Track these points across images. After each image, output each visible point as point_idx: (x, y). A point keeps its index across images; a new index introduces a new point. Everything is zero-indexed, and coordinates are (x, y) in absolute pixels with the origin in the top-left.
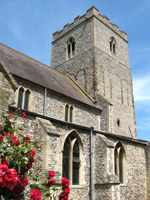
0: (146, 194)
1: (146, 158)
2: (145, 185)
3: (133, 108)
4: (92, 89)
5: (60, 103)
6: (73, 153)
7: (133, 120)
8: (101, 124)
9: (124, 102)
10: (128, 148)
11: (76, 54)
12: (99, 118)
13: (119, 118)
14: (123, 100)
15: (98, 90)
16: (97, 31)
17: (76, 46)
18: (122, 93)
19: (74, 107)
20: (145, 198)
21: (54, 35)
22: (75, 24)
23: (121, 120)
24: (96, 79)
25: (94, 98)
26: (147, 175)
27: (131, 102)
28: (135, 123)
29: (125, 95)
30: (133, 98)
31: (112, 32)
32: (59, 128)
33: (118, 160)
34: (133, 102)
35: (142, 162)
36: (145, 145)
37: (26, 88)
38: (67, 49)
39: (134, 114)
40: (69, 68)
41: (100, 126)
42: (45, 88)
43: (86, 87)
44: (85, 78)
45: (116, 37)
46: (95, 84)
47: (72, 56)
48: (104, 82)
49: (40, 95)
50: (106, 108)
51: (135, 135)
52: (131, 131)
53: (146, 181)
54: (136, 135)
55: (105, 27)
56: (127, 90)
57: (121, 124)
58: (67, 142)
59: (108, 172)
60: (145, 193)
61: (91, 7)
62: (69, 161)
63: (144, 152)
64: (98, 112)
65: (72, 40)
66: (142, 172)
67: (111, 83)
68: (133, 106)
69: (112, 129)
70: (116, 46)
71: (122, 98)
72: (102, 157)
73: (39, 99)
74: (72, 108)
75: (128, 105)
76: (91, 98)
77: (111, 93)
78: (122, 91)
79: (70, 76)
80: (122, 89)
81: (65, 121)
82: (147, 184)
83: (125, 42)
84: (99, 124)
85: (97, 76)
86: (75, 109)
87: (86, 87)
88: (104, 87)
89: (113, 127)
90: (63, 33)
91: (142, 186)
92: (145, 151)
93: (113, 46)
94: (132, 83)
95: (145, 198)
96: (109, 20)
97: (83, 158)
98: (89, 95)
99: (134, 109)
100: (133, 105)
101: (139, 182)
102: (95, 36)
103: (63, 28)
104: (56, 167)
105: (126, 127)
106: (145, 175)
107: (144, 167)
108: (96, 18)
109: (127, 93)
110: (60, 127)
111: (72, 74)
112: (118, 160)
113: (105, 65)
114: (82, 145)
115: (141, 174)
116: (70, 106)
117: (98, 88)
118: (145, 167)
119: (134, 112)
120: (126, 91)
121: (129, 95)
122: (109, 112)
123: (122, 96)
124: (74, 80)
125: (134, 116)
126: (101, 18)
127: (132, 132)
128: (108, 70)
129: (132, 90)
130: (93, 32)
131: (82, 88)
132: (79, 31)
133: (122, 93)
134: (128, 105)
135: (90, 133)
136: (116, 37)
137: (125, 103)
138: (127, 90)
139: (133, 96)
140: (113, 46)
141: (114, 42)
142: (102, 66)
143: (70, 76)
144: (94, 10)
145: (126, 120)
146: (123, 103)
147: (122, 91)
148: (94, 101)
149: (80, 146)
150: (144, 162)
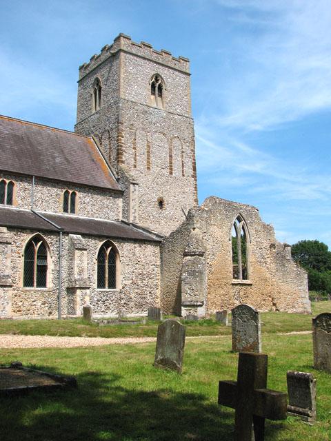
1: (161, 258)
2: (158, 292)
4: (116, 160)
5: (55, 191)
6: (38, 256)
8: (123, 210)
10: (124, 249)
11: (102, 106)
12: (120, 202)
13: (162, 198)
14: (171, 169)
15: (123, 162)
16: (126, 72)
17: (102, 92)
18: (171, 159)
19: (77, 192)
21: (81, 68)
22: (103, 58)
23: (165, 200)
24: (121, 146)
25: (117, 173)
27: (189, 171)
29: (177, 162)
30: (194, 163)
31: (157, 66)
32: (19, 233)
33: (64, 263)
34: (195, 169)
35: (154, 263)
36: (160, 242)
37: (8, 179)
38: (93, 95)
39: (195, 188)
40: (94, 127)
41: (121, 213)
42: (32, 176)
43: (110, 157)
44: (110, 144)
45: (164, 72)
46: (119, 154)
47: (98, 108)
48: (135, 148)
49: (26, 185)
50: (128, 188)
55: (142, 61)
56: (183, 152)
57: (165, 206)
58: (29, 248)
59: (75, 276)
61: (118, 35)
64: (118, 194)
65: (97, 81)
67: (149, 146)
68: (194, 176)
69: (135, 217)
70: (164, 87)
71: (171, 166)
72: (71, 260)
73: (25, 189)
74: (74, 194)
75: (183, 175)
76: (115, 173)
77: (148, 162)
78: (171, 156)
79: (95, 138)
81: (65, 210)
83: (184, 76)
84: (121, 210)
85: (123, 141)
86: (79, 195)
87: (110, 157)
88: (136, 155)
89: (136, 215)
90: (90, 69)
93: (157, 87)
94: (193, 141)
96: (151, 47)
97: (50, 263)
98: (112, 169)
99: (196, 180)
100: (196, 174)
101: (144, 288)
102: (122, 81)
103: (99, 53)
104: (7, 271)
107: (158, 270)
108: (125, 52)
109: (183, 156)
110: (20, 232)
111: (96, 136)
112: (64, 263)
113: (138, 124)
114: (49, 248)
116: (71, 192)
117: (124, 159)
122: (131, 194)
123: (171, 163)
124: (99, 144)
126: (134, 50)
128: (143, 129)
130: (119, 76)
131: (106, 157)
132: (104, 71)
133: (171, 159)
135: (59, 234)
136: (164, 72)
137: (177, 172)
139: (194, 160)
140: (157, 87)
141: (160, 82)
142: (132, 125)
143: (95, 138)
144: (123, 41)
146: (171, 173)
147: (171, 156)
148: (117, 177)
149: (47, 248)
150: (159, 263)
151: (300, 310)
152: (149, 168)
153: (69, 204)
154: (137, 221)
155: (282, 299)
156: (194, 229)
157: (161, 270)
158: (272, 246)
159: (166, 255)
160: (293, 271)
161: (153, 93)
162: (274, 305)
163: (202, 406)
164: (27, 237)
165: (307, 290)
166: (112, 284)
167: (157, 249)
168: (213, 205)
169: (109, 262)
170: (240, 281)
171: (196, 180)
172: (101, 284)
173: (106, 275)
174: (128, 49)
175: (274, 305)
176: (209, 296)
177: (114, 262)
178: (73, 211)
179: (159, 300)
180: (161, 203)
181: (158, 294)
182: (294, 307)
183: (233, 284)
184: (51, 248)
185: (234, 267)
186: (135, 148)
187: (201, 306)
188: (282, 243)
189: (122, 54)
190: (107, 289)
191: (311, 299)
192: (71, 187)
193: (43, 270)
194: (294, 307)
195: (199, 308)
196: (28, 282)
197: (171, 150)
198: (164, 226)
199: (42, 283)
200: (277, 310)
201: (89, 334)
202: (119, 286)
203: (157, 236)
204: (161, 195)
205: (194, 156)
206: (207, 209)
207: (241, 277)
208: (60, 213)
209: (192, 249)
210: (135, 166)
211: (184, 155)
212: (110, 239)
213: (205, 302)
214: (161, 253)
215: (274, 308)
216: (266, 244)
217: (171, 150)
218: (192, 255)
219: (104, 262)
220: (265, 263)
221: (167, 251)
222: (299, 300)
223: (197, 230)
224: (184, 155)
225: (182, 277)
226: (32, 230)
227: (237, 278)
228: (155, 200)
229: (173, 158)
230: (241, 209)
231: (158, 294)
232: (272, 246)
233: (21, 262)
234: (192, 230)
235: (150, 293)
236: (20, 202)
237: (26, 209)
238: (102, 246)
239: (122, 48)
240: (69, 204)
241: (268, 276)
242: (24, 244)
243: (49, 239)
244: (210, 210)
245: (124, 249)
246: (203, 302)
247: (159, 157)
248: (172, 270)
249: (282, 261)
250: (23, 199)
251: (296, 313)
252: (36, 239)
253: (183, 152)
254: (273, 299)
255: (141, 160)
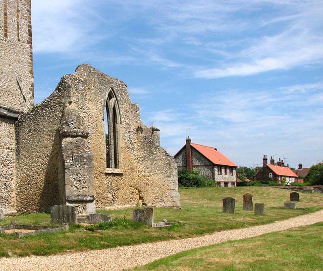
0: (15, 198)
1: (17, 140)
2: (13, 184)
3: (28, 45)
7: (27, 68)
9: (8, 33)
14: (6, 31)
18: (6, 18)
20: (12, 204)
26: (17, 168)
28: (31, 72)
29: (12, 22)
30: (30, 26)
34: (30, 34)
35: (8, 146)
36: (16, 119)
39: (31, 56)
51: (29, 96)
52: (22, 87)
53: (15, 177)
54: (33, 95)
56: (18, 11)
60: (12, 196)
62: (270, 42)
63: (13, 130)
66: (8, 162)
68: (30, 42)
71: (6, 27)
75: (19, 40)
78: (6, 14)
80: (5, 9)
82: (17, 182)
91: (5, 184)
92: (16, 129)
95: (12, 204)
100: (31, 39)
105: (10, 80)
106: (15, 168)
107: (13, 155)
109: (18, 16)
115: (5, 165)
118: (14, 154)
119: (31, 53)
120: (16, 14)
121: (22, 22)
123: (6, 23)
125: (31, 59)
127: (24, 91)
129: (29, 11)
133: (6, 18)
134: (19, 40)
137: (12, 36)
138: (18, 11)
139: (30, 22)
145: (10, 67)
146: (6, 36)
147: (6, 14)
150: (14, 146)
151: (169, 204)
155: (150, 192)
156: (70, 103)
157: (18, 155)
158: (139, 129)
159: (24, 136)
160: (162, 160)
162: (141, 198)
165: (177, 182)
167: (11, 128)
168: (88, 75)
170: (109, 170)
171: (31, 47)
175: (141, 198)
179: (14, 194)
181: (14, 186)
182: (162, 200)
183: (107, 174)
187: (91, 201)
188: (149, 127)
194: (162, 200)
195: (88, 205)
197: (5, 6)
200: (143, 204)
201: (18, 252)
203: (9, 110)
205: (29, 18)
206: (82, 79)
207: (113, 166)
209: (72, 128)
211: (20, 14)
213: (95, 196)
214: (17, 133)
215: (141, 202)
216: (133, 128)
217: (5, 6)
218: (73, 137)
220: (133, 149)
221: (27, 130)
222: (168, 193)
223: (73, 104)
225: (66, 164)
227: (108, 166)
229: (9, 17)
230: (112, 83)
231: (14, 186)
232: (139, 129)
234: (67, 104)
235: (5, 184)
241: (136, 164)
244: (86, 81)
246: (93, 197)
248: (35, 155)
249: (150, 148)
251: (164, 208)
254: (139, 192)
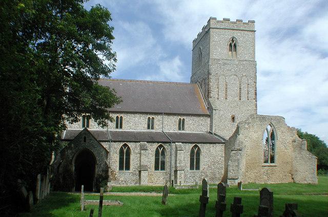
10: (204, 148)
27: (252, 95)
30: (256, 90)
45: (237, 34)
48: (218, 88)
56: (248, 84)
58: (157, 151)
67: (226, 85)
70: (237, 45)
78: (240, 89)
81: (180, 129)
97: (167, 160)
108: (213, 28)
109: (248, 87)
123: (240, 93)
136: (237, 34)
137: (243, 99)
140: (233, 46)
146: (240, 99)
147: (240, 89)
152: (226, 98)
153: (181, 125)
154: (217, 131)
161: (231, 50)
163: (51, 151)
164: (156, 146)
166: (198, 168)
169: (196, 156)
171: (256, 101)
172: (192, 168)
173: (195, 162)
174: (215, 26)
176: (247, 173)
177: (199, 156)
178: (183, 129)
180: (233, 118)
184: (167, 151)
185: (164, 157)
186: (218, 88)
189: (211, 30)
190: (195, 171)
191: (318, 174)
192: (181, 115)
193: (163, 163)
196: (157, 168)
198: (227, 134)
199: (163, 168)
202: (201, 169)
204: (234, 114)
205: (256, 86)
208: (177, 131)
210: (218, 99)
212: (197, 142)
219: (193, 156)
224: (249, 86)
226: (158, 142)
228: (230, 117)
233: (153, 159)
236: (157, 127)
237: (160, 131)
238: (192, 148)
239: (211, 27)
240: (181, 125)
242: (155, 149)
243: (166, 146)
245: (204, 148)
247: (234, 90)
250: (159, 125)
252: (161, 146)
253: (248, 84)
255: (222, 94)
